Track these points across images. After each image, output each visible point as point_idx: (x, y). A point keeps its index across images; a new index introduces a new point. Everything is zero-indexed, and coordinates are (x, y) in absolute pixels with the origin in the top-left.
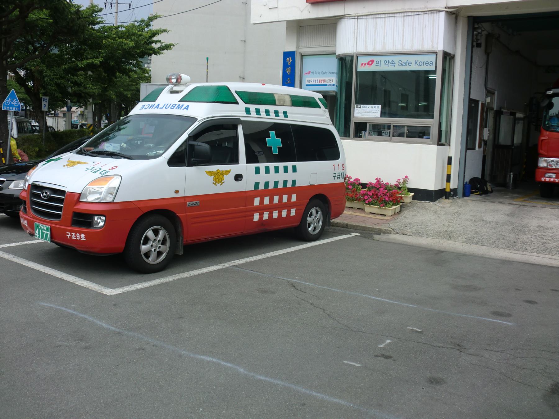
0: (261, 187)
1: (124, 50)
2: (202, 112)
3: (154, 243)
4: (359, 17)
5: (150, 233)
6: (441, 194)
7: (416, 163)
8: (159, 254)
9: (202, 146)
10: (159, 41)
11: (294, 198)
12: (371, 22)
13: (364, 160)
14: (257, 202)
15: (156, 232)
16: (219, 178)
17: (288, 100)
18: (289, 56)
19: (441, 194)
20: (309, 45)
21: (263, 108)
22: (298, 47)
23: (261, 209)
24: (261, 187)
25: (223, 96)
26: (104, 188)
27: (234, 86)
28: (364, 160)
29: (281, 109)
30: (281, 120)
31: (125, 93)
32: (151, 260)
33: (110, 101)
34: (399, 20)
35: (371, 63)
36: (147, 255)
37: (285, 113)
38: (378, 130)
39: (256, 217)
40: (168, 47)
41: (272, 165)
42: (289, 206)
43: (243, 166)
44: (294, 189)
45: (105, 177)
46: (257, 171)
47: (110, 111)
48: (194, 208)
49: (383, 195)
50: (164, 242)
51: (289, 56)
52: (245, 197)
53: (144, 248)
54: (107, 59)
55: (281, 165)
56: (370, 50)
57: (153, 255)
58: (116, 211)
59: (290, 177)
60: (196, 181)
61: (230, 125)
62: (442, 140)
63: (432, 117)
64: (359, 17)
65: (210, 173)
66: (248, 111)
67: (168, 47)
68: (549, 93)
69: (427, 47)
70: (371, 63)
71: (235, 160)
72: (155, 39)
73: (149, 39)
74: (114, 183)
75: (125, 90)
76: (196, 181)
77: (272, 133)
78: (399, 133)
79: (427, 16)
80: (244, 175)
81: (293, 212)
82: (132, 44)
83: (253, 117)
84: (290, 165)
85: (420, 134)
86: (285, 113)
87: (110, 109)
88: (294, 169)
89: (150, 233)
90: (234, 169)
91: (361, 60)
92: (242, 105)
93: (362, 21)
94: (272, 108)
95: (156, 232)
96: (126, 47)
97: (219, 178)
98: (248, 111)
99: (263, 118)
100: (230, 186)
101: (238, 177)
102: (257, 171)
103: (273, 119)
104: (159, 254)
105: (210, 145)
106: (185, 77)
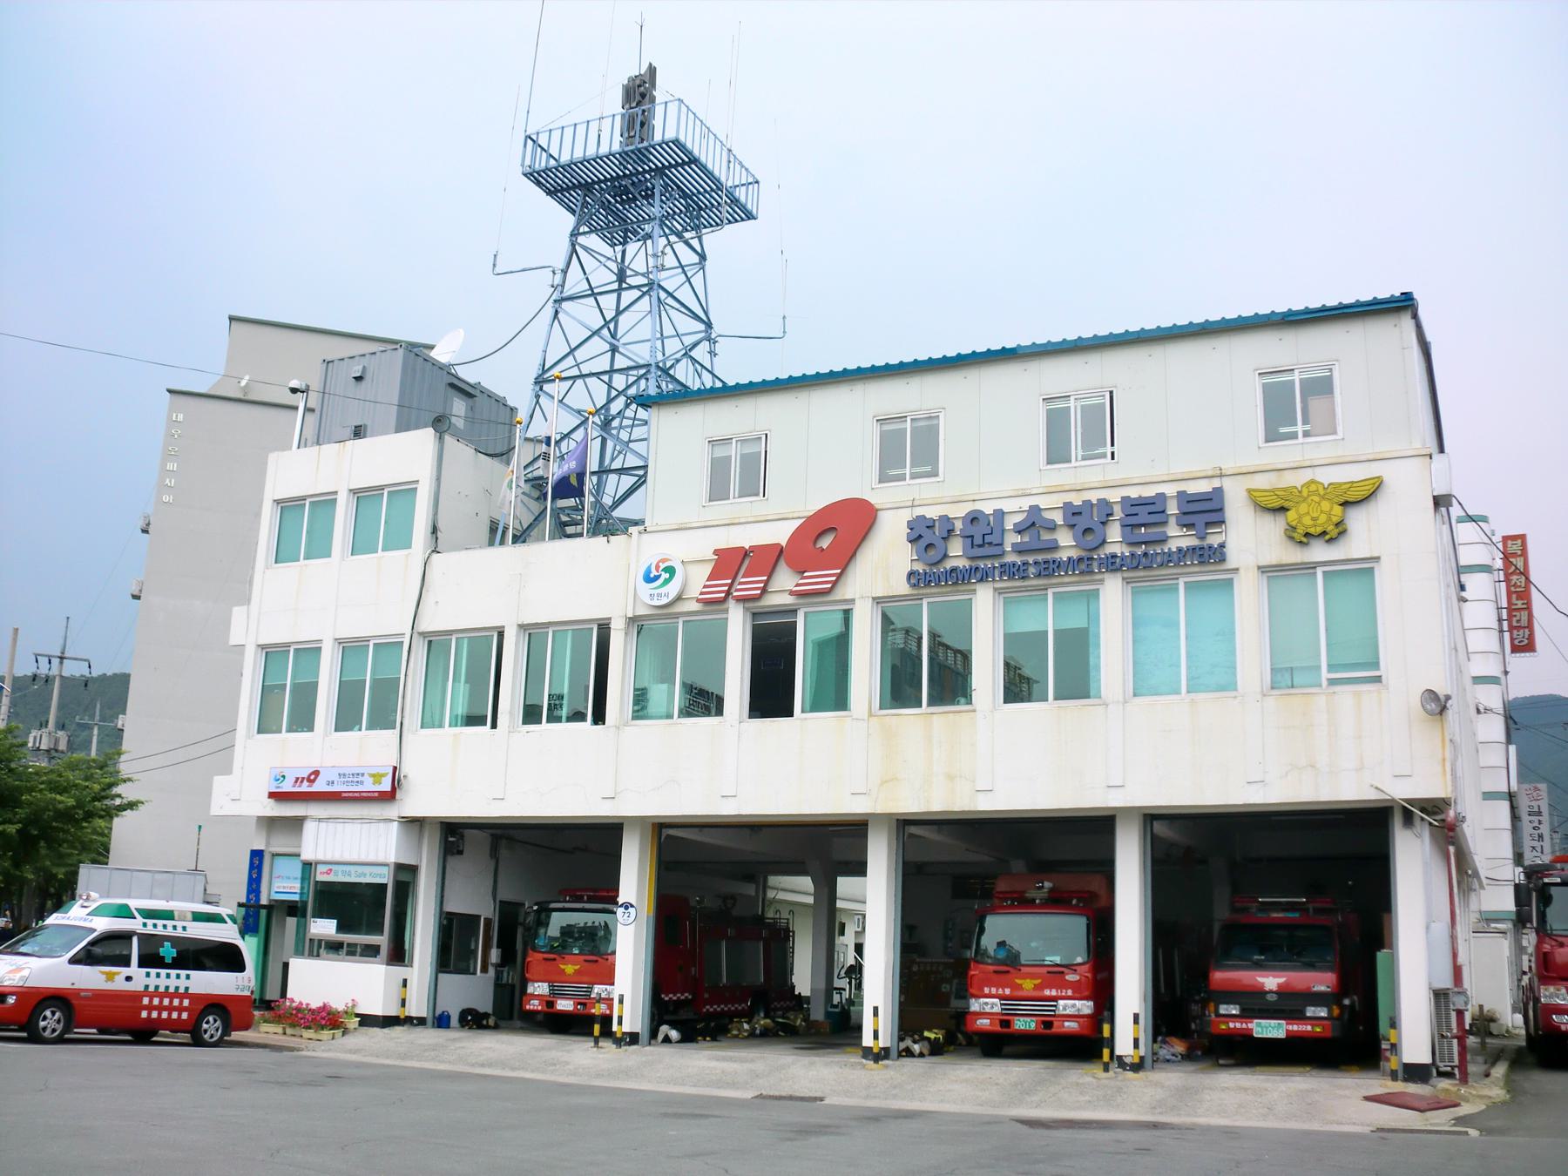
0: (151, 989)
1: (57, 811)
2: (103, 925)
3: (50, 1021)
4: (320, 820)
5: (48, 1013)
6: (421, 1022)
7: (358, 983)
8: (54, 1030)
9: (97, 950)
10: (119, 796)
11: (186, 1003)
12: (331, 826)
13: (316, 981)
14: (146, 1001)
15: (53, 1013)
16: (110, 977)
17: (190, 916)
18: (257, 855)
19: (421, 1022)
20: (280, 844)
21: (160, 923)
22: (268, 844)
23: (150, 1008)
24: (151, 989)
25: (124, 912)
26: (18, 975)
27: (134, 904)
28: (316, 981)
29: (180, 924)
30: (179, 933)
31: (54, 871)
32: (47, 1034)
33: (23, 882)
34: (357, 827)
35: (329, 872)
36: (44, 1029)
37: (184, 928)
38: (334, 947)
39: (144, 1014)
40: (132, 805)
41: (163, 972)
42: (180, 1009)
43: (134, 969)
44: (186, 995)
45: (19, 969)
46: (148, 975)
47: (20, 901)
48: (86, 998)
49: (328, 1020)
50: (59, 1021)
51: (257, 855)
52: (135, 997)
53: (42, 1024)
54: (28, 822)
55: (173, 972)
56: (329, 858)
57: (48, 1031)
58: (24, 994)
59: (182, 984)
60: (92, 978)
61: (125, 937)
62: (398, 955)
63: (381, 932)
64: (320, 820)
65: (106, 973)
66: (145, 925)
67: (132, 805)
68: (553, 905)
69: (381, 859)
70: (329, 872)
71: (128, 964)
72: (116, 790)
73: (105, 792)
74: (26, 973)
75: (53, 864)
76: (92, 978)
77: (167, 944)
78: (352, 951)
79: (382, 825)
80: (135, 978)
81: (185, 1016)
82: (71, 802)
83: (150, 930)
84: (183, 973)
85: (371, 951)
86: (184, 928)
87: (21, 896)
88: (188, 977)
89: (48, 1013)
90: (125, 971)
91: (321, 868)
92: (140, 920)
93: (323, 825)
94: (170, 923)
95: (53, 1013)
96: (61, 806)
97: (110, 977)
98: (145, 925)
99: (160, 931)
100: (119, 984)
101: (129, 979)
102: (148, 975)
103: (170, 932)
104: (54, 1030)
105: (105, 950)
106: (93, 895)
